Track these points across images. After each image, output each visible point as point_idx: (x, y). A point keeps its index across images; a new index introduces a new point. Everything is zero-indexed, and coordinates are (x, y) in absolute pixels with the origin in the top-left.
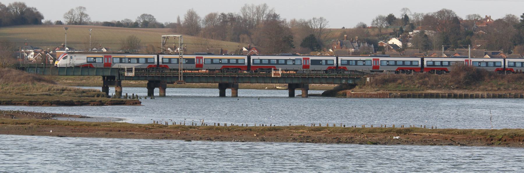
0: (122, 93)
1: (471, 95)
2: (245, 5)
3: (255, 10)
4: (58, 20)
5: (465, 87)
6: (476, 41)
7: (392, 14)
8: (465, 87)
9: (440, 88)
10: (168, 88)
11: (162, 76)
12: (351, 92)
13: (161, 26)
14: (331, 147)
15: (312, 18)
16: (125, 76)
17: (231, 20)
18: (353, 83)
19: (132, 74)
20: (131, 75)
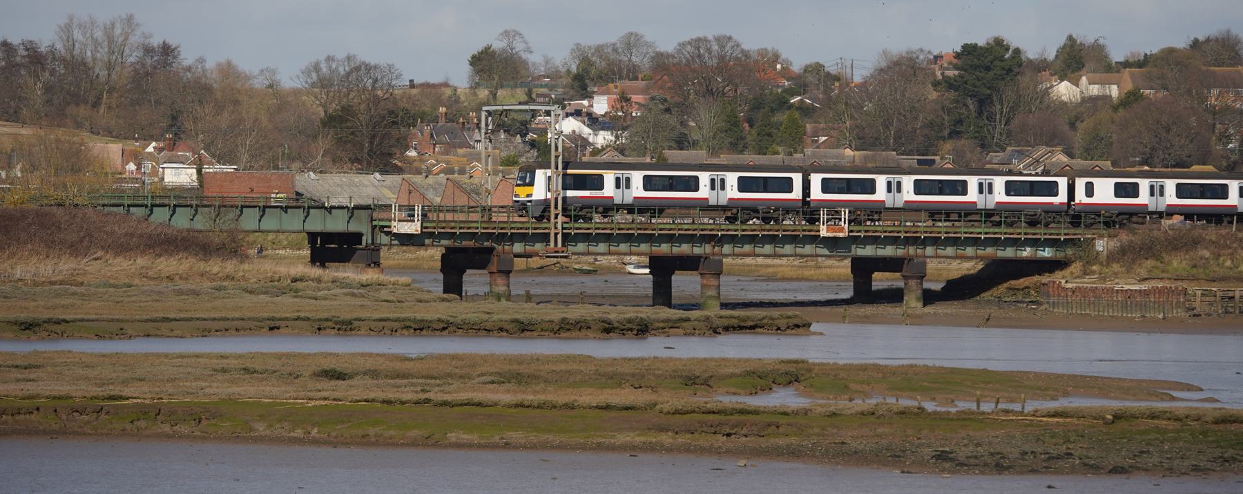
0: (873, 284)
3: (99, 34)
4: (808, 62)
7: (489, 48)
12: (1063, 284)
15: (322, 58)
17: (31, 62)
19: (414, 228)
20: (409, 232)
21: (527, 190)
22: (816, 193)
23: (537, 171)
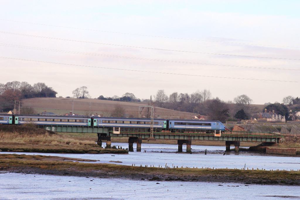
0: (178, 148)
2: (204, 91)
10: (193, 145)
13: (139, 101)
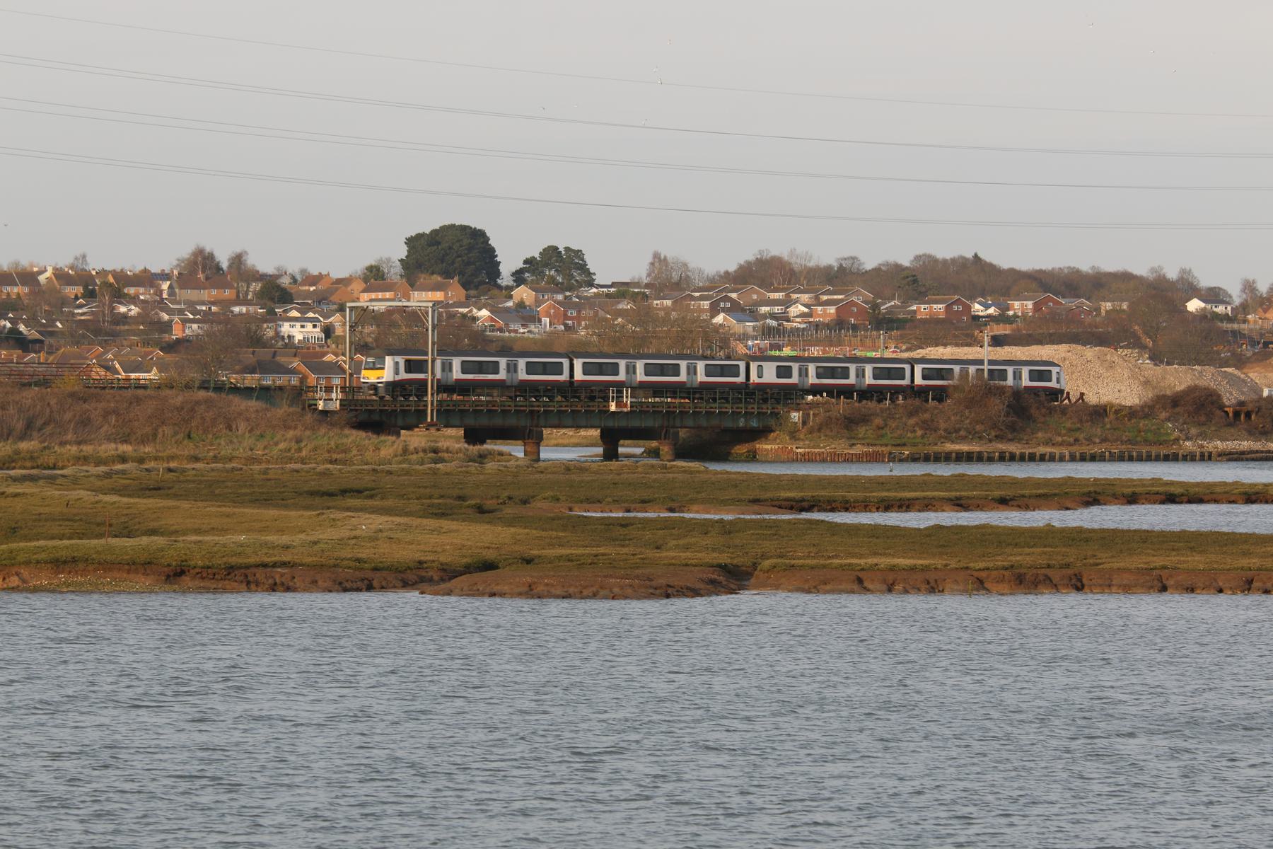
1: (1165, 455)
5: (1010, 436)
6: (586, 327)
8: (1010, 436)
9: (963, 439)
11: (489, 411)
12: (794, 449)
14: (331, 495)
16: (317, 409)
18: (759, 427)
21: (378, 373)
22: (919, 380)
23: (387, 357)
